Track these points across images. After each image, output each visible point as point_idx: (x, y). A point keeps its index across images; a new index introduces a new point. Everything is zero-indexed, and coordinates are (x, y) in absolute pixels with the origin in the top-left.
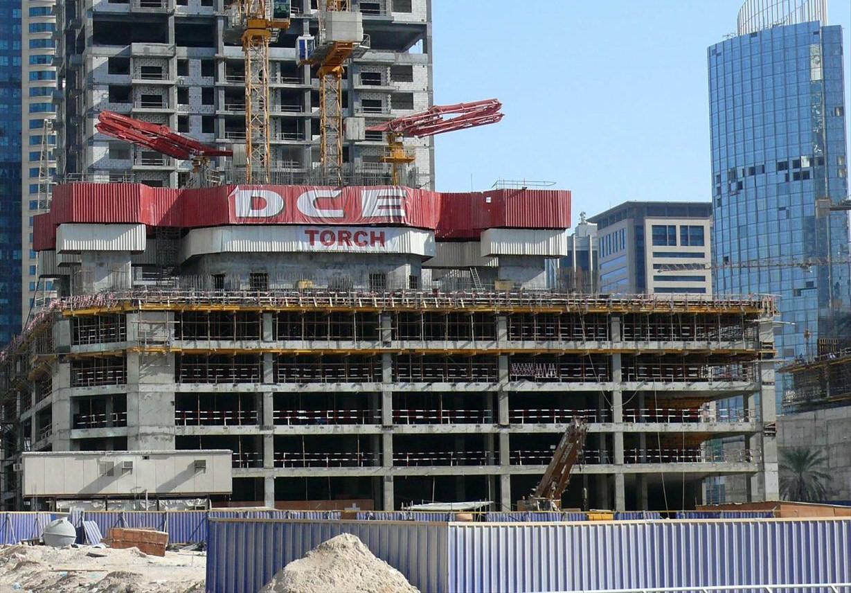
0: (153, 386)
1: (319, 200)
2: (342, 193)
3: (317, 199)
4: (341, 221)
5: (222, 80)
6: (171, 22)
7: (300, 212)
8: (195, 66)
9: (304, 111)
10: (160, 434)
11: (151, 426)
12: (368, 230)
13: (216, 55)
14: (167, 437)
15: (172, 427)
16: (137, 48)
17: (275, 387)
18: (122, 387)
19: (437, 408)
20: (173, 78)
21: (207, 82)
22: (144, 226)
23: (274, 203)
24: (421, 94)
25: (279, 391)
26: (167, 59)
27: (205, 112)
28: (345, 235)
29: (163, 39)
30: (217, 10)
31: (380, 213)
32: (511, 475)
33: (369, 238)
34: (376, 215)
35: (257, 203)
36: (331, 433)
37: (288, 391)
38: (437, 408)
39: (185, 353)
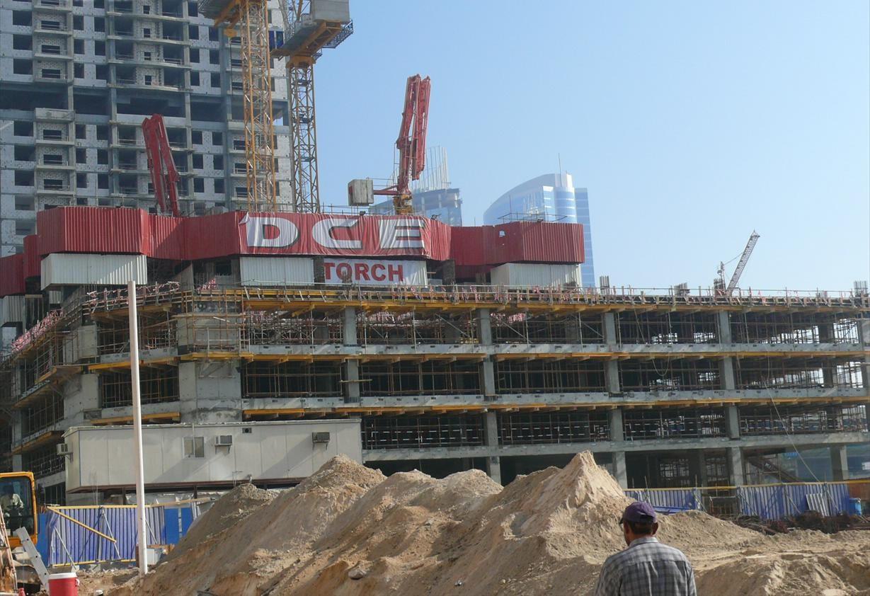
1: (335, 229)
2: (358, 222)
3: (333, 228)
4: (359, 253)
5: (116, 143)
6: (70, 91)
7: (315, 242)
8: (91, 131)
9: (187, 171)
10: (224, 409)
11: (211, 399)
12: (386, 263)
13: (110, 121)
16: (41, 112)
20: (71, 140)
21: (102, 144)
22: (144, 257)
24: (284, 159)
26: (66, 123)
27: (101, 171)
28: (362, 269)
29: (62, 105)
30: (110, 83)
31: (399, 244)
33: (386, 272)
34: (394, 247)
35: (270, 232)
39: (596, 407)
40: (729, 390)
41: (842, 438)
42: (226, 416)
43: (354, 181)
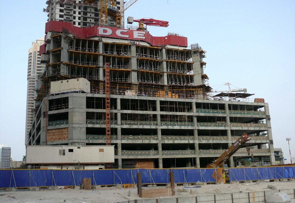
0: (78, 125)
10: (80, 142)
11: (77, 139)
14: (83, 144)
15: (85, 140)
17: (121, 126)
18: (66, 125)
19: (61, 104)
23: (109, 32)
25: (123, 127)
32: (200, 158)
35: (105, 31)
36: (141, 143)
37: (126, 128)
38: (61, 104)
40: (230, 140)
41: (262, 154)
42: (81, 144)
43: (129, 17)
